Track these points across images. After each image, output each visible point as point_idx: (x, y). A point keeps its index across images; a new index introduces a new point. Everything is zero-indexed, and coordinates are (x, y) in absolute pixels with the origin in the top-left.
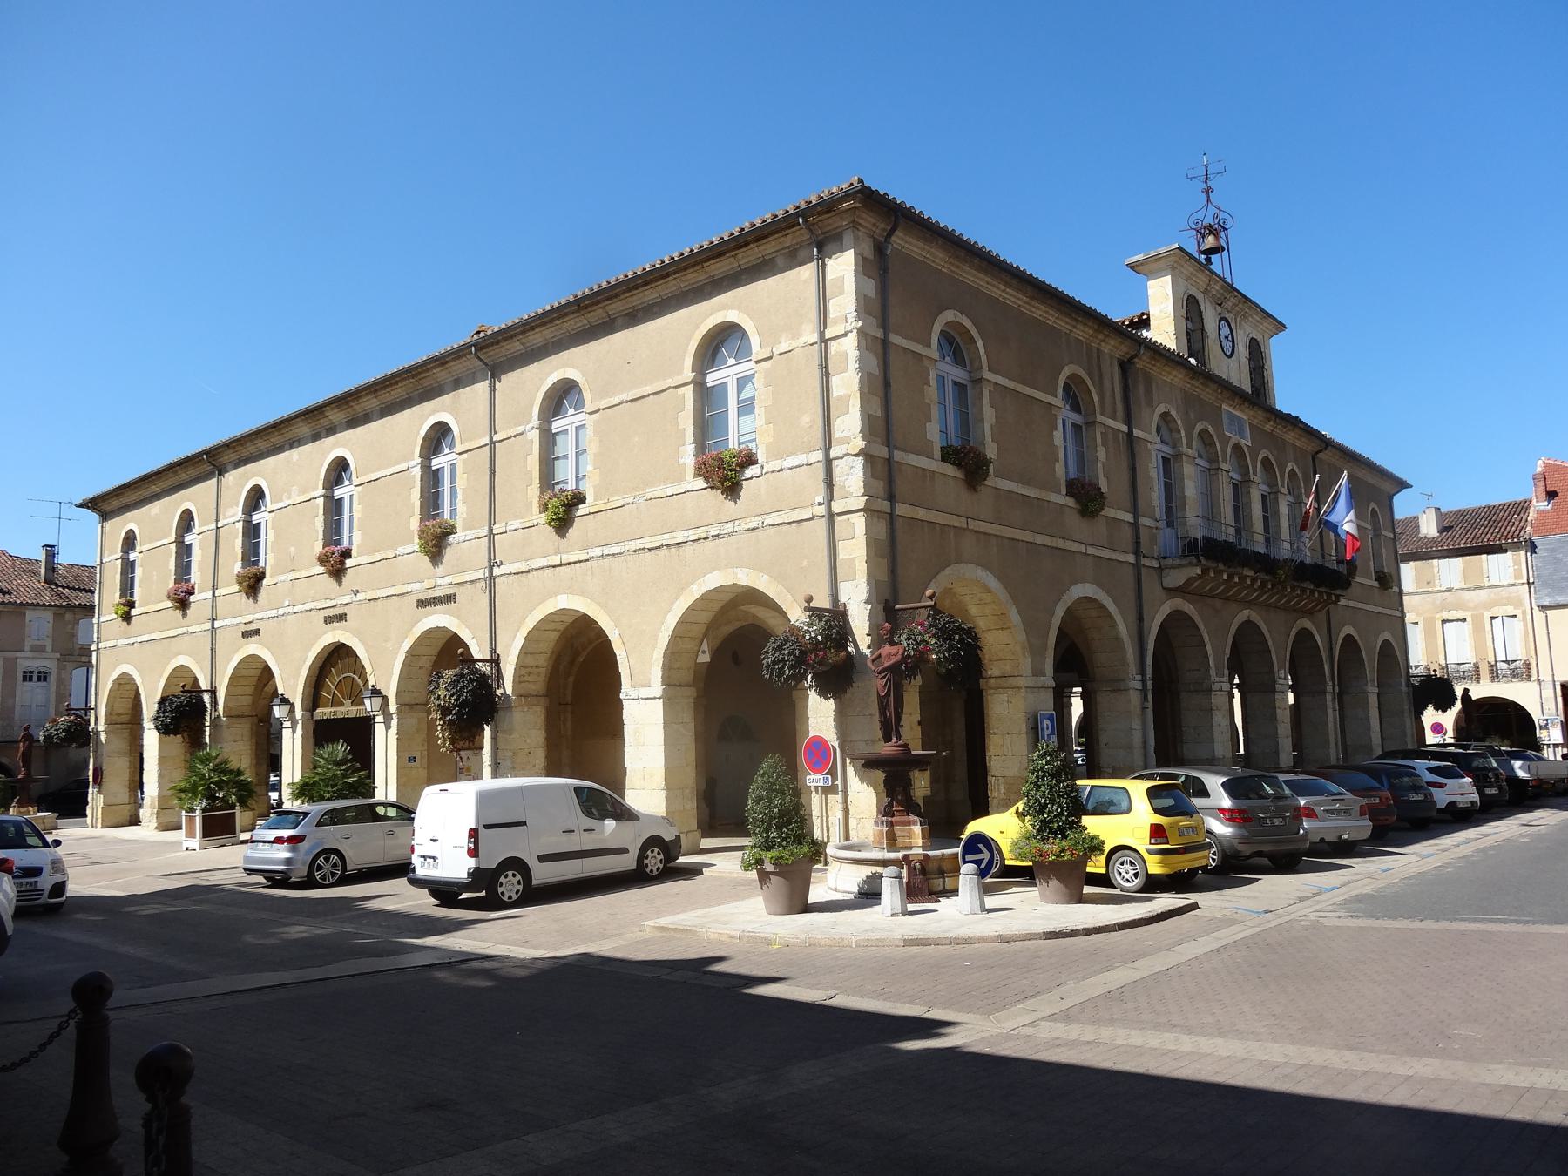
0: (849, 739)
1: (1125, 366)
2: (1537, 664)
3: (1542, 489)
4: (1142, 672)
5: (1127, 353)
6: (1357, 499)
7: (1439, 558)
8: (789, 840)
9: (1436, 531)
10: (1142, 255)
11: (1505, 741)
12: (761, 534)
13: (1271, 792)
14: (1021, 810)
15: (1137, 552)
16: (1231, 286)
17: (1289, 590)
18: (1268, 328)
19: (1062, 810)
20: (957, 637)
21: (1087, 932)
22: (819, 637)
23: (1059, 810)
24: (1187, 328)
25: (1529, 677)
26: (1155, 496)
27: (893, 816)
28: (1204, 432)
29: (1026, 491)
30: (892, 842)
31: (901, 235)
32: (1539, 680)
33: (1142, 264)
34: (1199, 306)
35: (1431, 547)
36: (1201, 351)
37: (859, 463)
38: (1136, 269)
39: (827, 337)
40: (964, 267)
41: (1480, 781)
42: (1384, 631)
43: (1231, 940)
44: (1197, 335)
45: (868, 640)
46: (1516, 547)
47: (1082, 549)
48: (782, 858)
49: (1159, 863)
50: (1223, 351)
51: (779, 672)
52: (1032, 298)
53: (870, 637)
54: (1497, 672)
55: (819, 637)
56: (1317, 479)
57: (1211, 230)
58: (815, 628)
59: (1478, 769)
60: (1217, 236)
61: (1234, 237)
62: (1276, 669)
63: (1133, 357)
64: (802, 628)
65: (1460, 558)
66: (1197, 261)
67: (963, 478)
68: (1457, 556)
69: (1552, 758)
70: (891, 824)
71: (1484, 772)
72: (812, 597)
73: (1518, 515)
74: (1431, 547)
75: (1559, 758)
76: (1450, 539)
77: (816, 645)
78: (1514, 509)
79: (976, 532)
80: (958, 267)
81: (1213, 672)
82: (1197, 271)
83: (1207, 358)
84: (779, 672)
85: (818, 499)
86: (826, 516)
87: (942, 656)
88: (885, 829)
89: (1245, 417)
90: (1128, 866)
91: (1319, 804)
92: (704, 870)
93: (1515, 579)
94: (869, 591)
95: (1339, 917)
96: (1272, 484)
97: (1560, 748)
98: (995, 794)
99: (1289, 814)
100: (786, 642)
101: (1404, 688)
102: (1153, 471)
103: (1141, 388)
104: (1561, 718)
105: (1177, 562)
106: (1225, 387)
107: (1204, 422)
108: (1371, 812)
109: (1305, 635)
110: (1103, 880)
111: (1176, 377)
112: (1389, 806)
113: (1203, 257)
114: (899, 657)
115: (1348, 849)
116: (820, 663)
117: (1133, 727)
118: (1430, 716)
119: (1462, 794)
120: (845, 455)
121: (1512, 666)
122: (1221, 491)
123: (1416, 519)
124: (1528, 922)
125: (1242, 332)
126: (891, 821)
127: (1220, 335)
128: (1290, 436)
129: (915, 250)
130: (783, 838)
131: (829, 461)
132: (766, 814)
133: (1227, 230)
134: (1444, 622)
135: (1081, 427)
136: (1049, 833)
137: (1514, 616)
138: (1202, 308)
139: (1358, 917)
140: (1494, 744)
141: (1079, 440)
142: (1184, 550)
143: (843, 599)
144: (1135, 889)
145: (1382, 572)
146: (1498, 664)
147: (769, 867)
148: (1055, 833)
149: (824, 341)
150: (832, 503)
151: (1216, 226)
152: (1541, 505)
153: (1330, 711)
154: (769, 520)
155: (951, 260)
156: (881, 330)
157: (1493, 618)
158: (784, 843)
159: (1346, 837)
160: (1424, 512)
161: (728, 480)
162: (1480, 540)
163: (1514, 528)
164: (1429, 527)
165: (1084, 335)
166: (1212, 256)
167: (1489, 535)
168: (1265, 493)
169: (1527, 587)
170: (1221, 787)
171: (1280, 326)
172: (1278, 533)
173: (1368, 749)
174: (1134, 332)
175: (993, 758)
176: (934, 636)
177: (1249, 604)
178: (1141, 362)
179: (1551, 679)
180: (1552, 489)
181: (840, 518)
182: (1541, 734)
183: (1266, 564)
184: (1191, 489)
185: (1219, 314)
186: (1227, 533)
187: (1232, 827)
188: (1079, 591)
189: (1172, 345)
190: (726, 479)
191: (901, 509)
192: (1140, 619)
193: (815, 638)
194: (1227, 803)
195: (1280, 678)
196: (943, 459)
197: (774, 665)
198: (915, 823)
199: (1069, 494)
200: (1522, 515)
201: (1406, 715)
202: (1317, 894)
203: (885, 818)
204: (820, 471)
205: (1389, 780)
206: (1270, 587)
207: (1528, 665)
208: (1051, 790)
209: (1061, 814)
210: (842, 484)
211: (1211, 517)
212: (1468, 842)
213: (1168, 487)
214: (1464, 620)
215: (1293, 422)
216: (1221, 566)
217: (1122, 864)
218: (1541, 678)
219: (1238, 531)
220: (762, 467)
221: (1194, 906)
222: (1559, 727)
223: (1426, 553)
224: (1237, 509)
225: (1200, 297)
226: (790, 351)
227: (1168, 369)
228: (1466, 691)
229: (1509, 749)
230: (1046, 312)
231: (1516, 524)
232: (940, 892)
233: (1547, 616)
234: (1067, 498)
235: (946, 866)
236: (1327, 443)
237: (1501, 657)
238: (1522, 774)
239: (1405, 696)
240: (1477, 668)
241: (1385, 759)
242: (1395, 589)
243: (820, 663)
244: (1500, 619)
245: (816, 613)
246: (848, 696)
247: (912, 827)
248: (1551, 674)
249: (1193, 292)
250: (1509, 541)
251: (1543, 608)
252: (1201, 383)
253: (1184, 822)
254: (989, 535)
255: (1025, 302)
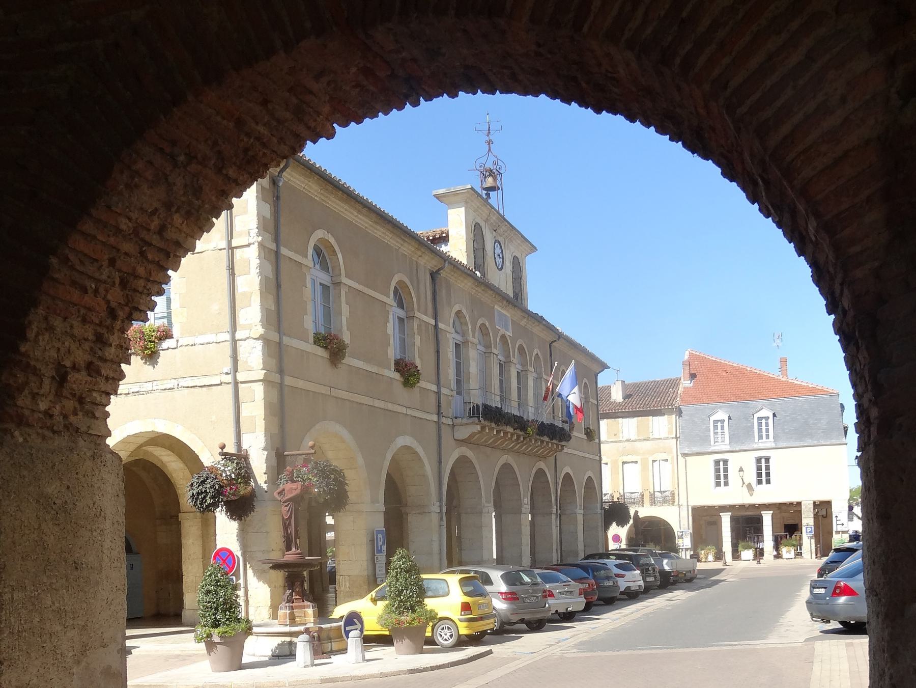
0: (249, 550)
1: (434, 275)
2: (679, 494)
3: (687, 372)
4: (440, 501)
5: (435, 266)
6: (577, 379)
7: (623, 417)
8: (231, 620)
9: (621, 398)
10: (445, 189)
11: (657, 547)
12: (176, 394)
13: (529, 581)
14: (373, 597)
15: (439, 413)
16: (503, 217)
17: (533, 442)
18: (525, 250)
19: (413, 594)
20: (333, 476)
21: (433, 668)
22: (233, 476)
23: (411, 594)
24: (474, 247)
25: (674, 502)
26: (450, 373)
27: (293, 602)
28: (483, 325)
29: (368, 368)
30: (293, 620)
31: (290, 171)
32: (679, 504)
33: (444, 196)
34: (482, 231)
35: (618, 410)
36: (483, 264)
37: (259, 345)
38: (440, 199)
39: (233, 246)
40: (331, 197)
41: (645, 572)
42: (588, 471)
43: (518, 667)
44: (480, 253)
45: (265, 477)
46: (670, 412)
47: (404, 410)
48: (226, 632)
49: (466, 627)
50: (496, 265)
51: (202, 500)
52: (376, 222)
53: (266, 475)
54: (654, 499)
55: (233, 476)
56: (556, 365)
57: (491, 173)
58: (229, 468)
59: (643, 565)
60: (495, 179)
61: (507, 181)
62: (522, 497)
63: (439, 270)
64: (220, 468)
65: (636, 418)
66: (481, 196)
67: (329, 357)
68: (634, 416)
69: (684, 557)
70: (292, 608)
71: (647, 567)
72: (225, 445)
73: (673, 389)
74: (618, 410)
75: (688, 557)
76: (630, 404)
77: (230, 481)
78: (670, 385)
79: (336, 398)
80: (327, 197)
81: (484, 500)
82: (482, 206)
83: (486, 270)
84: (202, 500)
85: (226, 370)
86: (233, 383)
87: (322, 490)
88: (288, 612)
89: (508, 315)
90: (446, 631)
91: (555, 588)
92: (132, 650)
93: (668, 434)
94: (266, 441)
95: (574, 653)
96: (524, 365)
97: (689, 551)
98: (342, 588)
99: (540, 594)
100: (207, 478)
101: (599, 511)
102: (449, 354)
103: (444, 291)
104: (691, 531)
105: (465, 421)
106: (498, 294)
107: (483, 318)
108: (584, 593)
109: (541, 473)
110: (431, 641)
111: (466, 285)
112: (593, 589)
113: (484, 192)
114: (298, 491)
115: (568, 617)
116: (234, 495)
117: (434, 539)
118: (614, 529)
119: (634, 581)
120: (248, 338)
121: (664, 495)
122: (492, 369)
123: (609, 387)
124: (672, 648)
125: (508, 251)
126: (292, 606)
127: (494, 253)
128: (537, 330)
129: (297, 182)
130: (227, 619)
131: (234, 342)
132: (214, 603)
133: (501, 174)
134: (624, 463)
135: (404, 319)
136: (404, 609)
137: (667, 460)
138: (484, 233)
139: (584, 652)
140: (652, 549)
141: (402, 330)
142: (470, 414)
143: (245, 446)
144: (450, 645)
145: (589, 428)
146: (656, 493)
147: (216, 639)
148: (407, 609)
149: (231, 249)
150: (237, 373)
151: (495, 171)
152: (686, 383)
153: (554, 527)
154: (183, 383)
155: (322, 192)
156: (275, 244)
157: (654, 461)
158: (228, 622)
159: (570, 609)
160: (615, 384)
161: (148, 349)
162: (648, 406)
163: (669, 398)
164: (617, 395)
165: (408, 251)
166: (490, 193)
167: (654, 403)
168: (518, 371)
169: (675, 440)
170: (500, 579)
171: (534, 249)
172: (527, 400)
173: (576, 554)
174: (435, 247)
175: (342, 562)
176: (316, 475)
177: (507, 451)
178: (444, 273)
179: (686, 505)
180: (693, 372)
181: (243, 385)
182: (679, 542)
183: (520, 424)
184: (474, 368)
185: (495, 237)
186: (495, 402)
187: (506, 604)
188: (404, 441)
189: (464, 261)
190: (146, 348)
191: (288, 381)
192: (440, 462)
193: (230, 475)
194: (504, 588)
195: (525, 504)
196: (315, 343)
197: (198, 495)
198: (308, 607)
199: (397, 370)
200: (674, 389)
201: (600, 529)
202: (558, 643)
203: (287, 604)
204: (227, 348)
205: (593, 574)
206: (522, 440)
207: (673, 494)
208: (406, 581)
209: (412, 596)
210: (245, 360)
211: (485, 388)
212: (638, 610)
213: (458, 364)
214: (636, 462)
215: (539, 319)
216: (493, 425)
217: (443, 629)
218: (680, 504)
219: (502, 399)
220: (177, 341)
221: (490, 652)
222: (689, 535)
223: (615, 414)
224: (501, 381)
225: (483, 224)
226: (201, 252)
227: (462, 279)
228: (636, 512)
229: (660, 552)
230: (384, 233)
231: (671, 395)
232: (329, 652)
233: (686, 461)
234: (395, 372)
235: (332, 635)
236: (560, 336)
237: (657, 489)
238: (667, 568)
239: (600, 516)
240: (642, 496)
241: (587, 560)
242: (597, 441)
243: (234, 495)
244: (658, 462)
245: (226, 456)
246: (248, 519)
247: (307, 610)
248: (686, 500)
249: (479, 220)
250: (666, 407)
251: (684, 455)
252: (483, 290)
253: (481, 600)
254: (345, 400)
255: (371, 226)
